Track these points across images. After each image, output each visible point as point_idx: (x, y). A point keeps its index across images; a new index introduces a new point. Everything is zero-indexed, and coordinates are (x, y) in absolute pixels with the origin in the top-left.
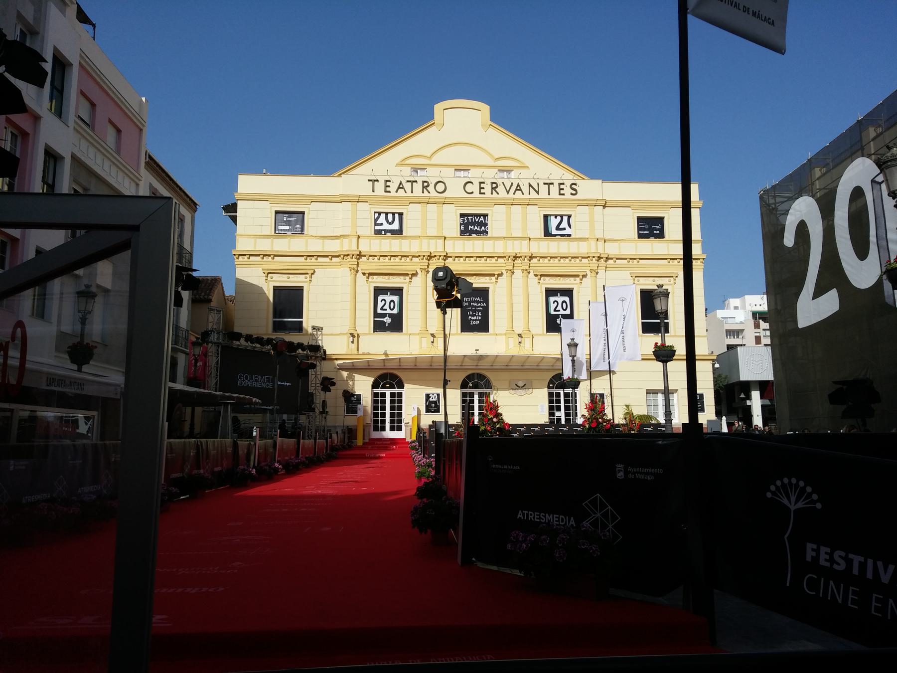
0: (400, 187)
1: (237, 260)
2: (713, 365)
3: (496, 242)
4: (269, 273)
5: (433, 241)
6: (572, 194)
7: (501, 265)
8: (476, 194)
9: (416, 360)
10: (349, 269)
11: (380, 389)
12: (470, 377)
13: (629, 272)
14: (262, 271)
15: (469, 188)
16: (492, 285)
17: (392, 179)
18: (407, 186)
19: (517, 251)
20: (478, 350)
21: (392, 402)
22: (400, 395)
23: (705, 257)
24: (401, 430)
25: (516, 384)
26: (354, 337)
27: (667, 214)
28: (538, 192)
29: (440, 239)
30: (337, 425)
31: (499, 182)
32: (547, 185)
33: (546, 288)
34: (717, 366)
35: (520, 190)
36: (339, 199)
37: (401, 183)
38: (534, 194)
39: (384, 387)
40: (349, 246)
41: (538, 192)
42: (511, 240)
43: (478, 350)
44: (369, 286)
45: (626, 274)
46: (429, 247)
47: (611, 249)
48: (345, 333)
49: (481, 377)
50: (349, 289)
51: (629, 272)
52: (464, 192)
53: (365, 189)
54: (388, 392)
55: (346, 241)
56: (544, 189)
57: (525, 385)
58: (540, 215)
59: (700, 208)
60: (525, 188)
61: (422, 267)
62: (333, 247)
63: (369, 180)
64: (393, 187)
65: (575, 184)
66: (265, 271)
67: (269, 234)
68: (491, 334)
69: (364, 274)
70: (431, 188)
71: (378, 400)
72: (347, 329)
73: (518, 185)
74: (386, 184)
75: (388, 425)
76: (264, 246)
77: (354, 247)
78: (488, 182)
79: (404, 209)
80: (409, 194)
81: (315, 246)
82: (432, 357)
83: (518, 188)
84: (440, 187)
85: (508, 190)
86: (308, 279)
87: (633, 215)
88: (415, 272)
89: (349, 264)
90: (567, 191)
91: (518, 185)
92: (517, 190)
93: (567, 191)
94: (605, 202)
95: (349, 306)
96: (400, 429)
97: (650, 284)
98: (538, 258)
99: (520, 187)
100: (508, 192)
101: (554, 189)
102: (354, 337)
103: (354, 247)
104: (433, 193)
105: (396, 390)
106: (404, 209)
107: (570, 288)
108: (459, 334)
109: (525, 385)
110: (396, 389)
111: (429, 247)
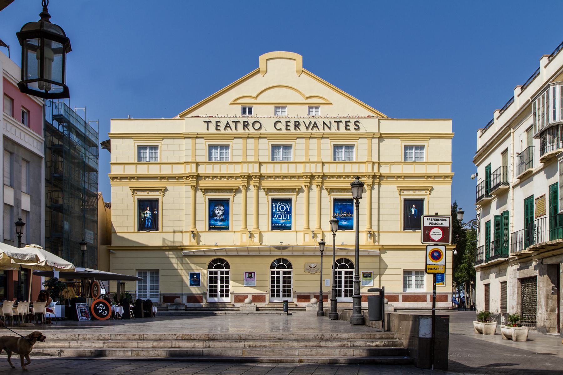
0: (228, 126)
1: (111, 181)
2: (453, 252)
3: (222, 165)
4: (401, 189)
5: (251, 165)
6: (355, 129)
7: (239, 183)
8: (284, 131)
9: (293, 248)
10: (190, 186)
11: (349, 271)
12: (215, 261)
13: (396, 186)
14: (129, 188)
15: (279, 126)
16: (294, 196)
17: (221, 120)
18: (233, 126)
19: (313, 171)
20: (282, 243)
21: (222, 278)
22: (227, 273)
23: (453, 175)
24: (279, 297)
25: (310, 266)
26: (195, 235)
27: (427, 143)
28: (330, 128)
29: (449, 164)
30: (183, 293)
31: (301, 121)
32: (235, 124)
33: (138, 199)
34: (455, 252)
35: (317, 127)
36: (183, 136)
37: (228, 123)
38: (327, 130)
39: (278, 268)
40: (190, 169)
41: (330, 128)
42: (328, 164)
43: (282, 243)
44: (268, 197)
45: (127, 189)
46: (310, 170)
47: (385, 170)
48: (188, 231)
49: (222, 261)
50: (191, 200)
51: (396, 186)
52: (275, 128)
53: (202, 129)
54: (281, 271)
55: (188, 166)
56: (335, 125)
57: (316, 266)
58: (205, 144)
59: (452, 138)
60: (320, 126)
61: (243, 184)
62: (179, 170)
63: (204, 121)
64: (222, 126)
65: (358, 122)
66: (398, 188)
67: (133, 162)
68: (293, 231)
69: (327, 189)
70: (250, 127)
71: (212, 278)
72: (190, 228)
73: (315, 123)
74: (216, 124)
75: (343, 293)
76: (397, 170)
77: (194, 171)
78: (293, 121)
79: (158, 142)
80: (234, 131)
81: (166, 170)
82: (304, 247)
83: (315, 125)
84: (257, 126)
85: (325, 126)
86: (162, 194)
87: (331, 144)
88: (238, 188)
89: (190, 182)
90: (352, 127)
91: (315, 123)
92: (314, 126)
93: (352, 127)
94: (379, 135)
95: (191, 212)
96: (227, 296)
97: (411, 195)
98: (396, 177)
99: (316, 125)
100: (307, 128)
101: (342, 126)
102: (195, 235)
103: (194, 171)
104: (252, 130)
105: (225, 270)
106: (158, 142)
107: (289, 198)
108: (402, 232)
109: (316, 266)
110: (225, 269)
111: (310, 170)
